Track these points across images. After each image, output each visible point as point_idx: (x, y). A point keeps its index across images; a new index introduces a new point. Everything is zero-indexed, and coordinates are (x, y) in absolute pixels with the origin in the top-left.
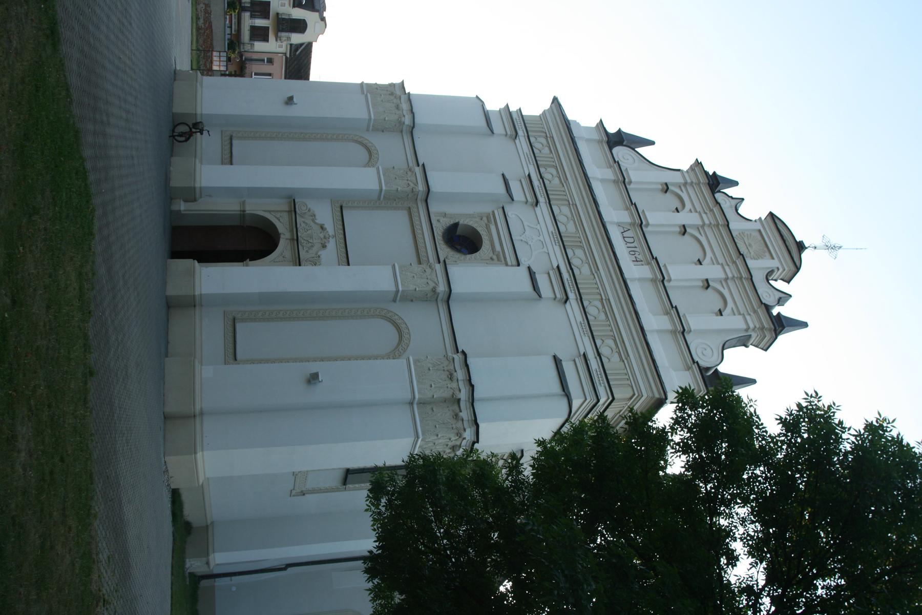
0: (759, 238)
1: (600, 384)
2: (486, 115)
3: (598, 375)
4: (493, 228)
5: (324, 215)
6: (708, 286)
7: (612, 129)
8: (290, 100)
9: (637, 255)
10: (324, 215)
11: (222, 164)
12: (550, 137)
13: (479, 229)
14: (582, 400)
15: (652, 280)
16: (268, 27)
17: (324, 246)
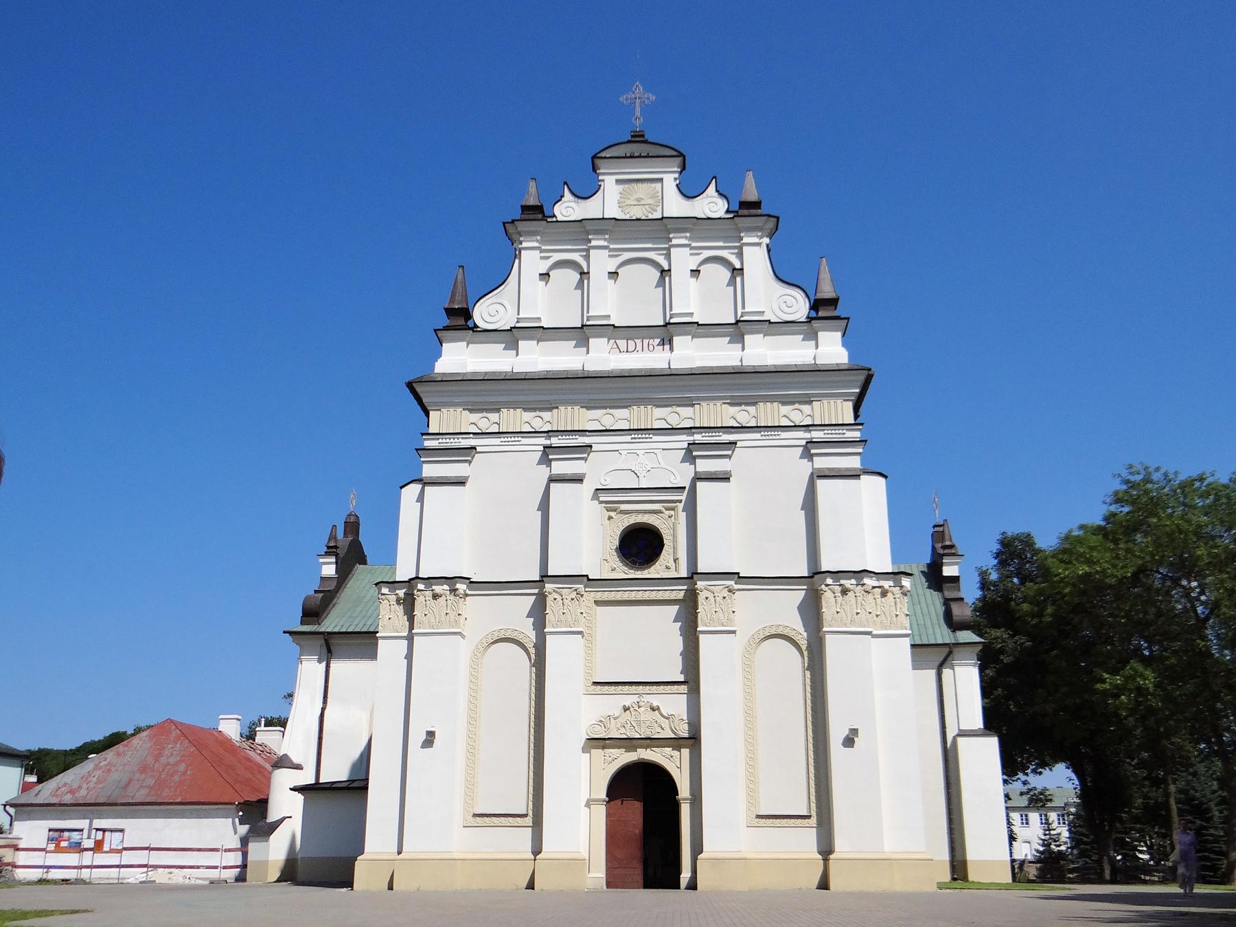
1: (778, 435)
3: (832, 434)
4: (624, 507)
6: (616, 273)
12: (472, 405)
16: (240, 824)
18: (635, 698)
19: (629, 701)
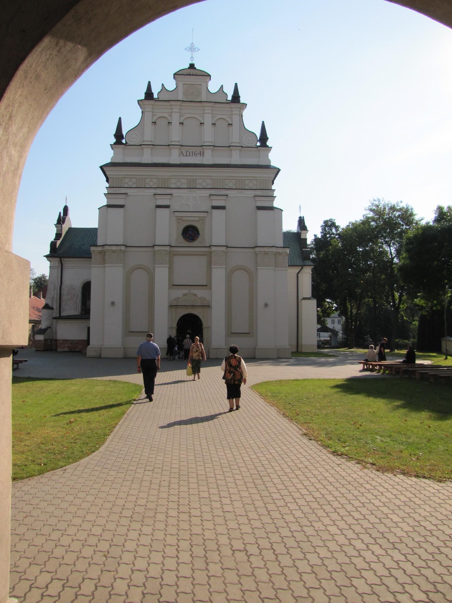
2: (108, 206)
4: (185, 218)
5: (179, 293)
7: (114, 140)
8: (113, 303)
9: (197, 153)
10: (179, 293)
15: (151, 149)
17: (196, 295)
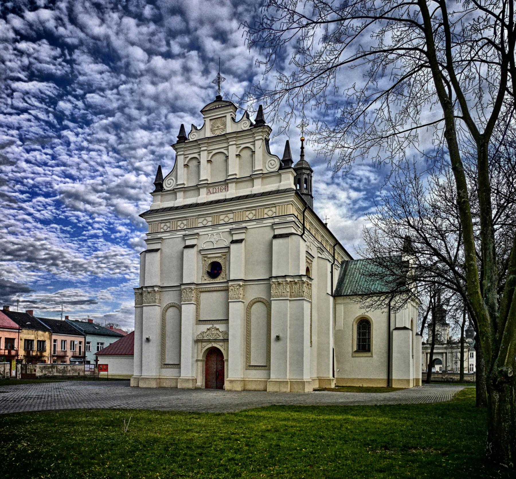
0: (214, 121)
4: (209, 256)
5: (204, 328)
6: (239, 155)
11: (133, 355)
13: (210, 262)
14: (292, 228)
18: (211, 326)
19: (209, 326)
